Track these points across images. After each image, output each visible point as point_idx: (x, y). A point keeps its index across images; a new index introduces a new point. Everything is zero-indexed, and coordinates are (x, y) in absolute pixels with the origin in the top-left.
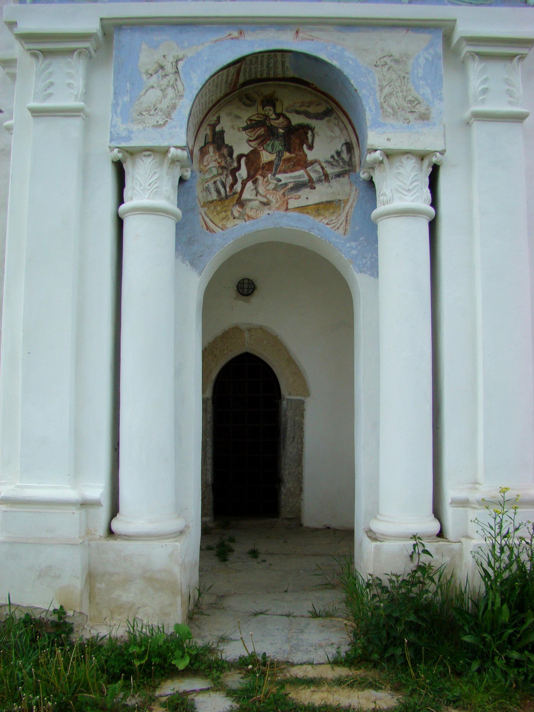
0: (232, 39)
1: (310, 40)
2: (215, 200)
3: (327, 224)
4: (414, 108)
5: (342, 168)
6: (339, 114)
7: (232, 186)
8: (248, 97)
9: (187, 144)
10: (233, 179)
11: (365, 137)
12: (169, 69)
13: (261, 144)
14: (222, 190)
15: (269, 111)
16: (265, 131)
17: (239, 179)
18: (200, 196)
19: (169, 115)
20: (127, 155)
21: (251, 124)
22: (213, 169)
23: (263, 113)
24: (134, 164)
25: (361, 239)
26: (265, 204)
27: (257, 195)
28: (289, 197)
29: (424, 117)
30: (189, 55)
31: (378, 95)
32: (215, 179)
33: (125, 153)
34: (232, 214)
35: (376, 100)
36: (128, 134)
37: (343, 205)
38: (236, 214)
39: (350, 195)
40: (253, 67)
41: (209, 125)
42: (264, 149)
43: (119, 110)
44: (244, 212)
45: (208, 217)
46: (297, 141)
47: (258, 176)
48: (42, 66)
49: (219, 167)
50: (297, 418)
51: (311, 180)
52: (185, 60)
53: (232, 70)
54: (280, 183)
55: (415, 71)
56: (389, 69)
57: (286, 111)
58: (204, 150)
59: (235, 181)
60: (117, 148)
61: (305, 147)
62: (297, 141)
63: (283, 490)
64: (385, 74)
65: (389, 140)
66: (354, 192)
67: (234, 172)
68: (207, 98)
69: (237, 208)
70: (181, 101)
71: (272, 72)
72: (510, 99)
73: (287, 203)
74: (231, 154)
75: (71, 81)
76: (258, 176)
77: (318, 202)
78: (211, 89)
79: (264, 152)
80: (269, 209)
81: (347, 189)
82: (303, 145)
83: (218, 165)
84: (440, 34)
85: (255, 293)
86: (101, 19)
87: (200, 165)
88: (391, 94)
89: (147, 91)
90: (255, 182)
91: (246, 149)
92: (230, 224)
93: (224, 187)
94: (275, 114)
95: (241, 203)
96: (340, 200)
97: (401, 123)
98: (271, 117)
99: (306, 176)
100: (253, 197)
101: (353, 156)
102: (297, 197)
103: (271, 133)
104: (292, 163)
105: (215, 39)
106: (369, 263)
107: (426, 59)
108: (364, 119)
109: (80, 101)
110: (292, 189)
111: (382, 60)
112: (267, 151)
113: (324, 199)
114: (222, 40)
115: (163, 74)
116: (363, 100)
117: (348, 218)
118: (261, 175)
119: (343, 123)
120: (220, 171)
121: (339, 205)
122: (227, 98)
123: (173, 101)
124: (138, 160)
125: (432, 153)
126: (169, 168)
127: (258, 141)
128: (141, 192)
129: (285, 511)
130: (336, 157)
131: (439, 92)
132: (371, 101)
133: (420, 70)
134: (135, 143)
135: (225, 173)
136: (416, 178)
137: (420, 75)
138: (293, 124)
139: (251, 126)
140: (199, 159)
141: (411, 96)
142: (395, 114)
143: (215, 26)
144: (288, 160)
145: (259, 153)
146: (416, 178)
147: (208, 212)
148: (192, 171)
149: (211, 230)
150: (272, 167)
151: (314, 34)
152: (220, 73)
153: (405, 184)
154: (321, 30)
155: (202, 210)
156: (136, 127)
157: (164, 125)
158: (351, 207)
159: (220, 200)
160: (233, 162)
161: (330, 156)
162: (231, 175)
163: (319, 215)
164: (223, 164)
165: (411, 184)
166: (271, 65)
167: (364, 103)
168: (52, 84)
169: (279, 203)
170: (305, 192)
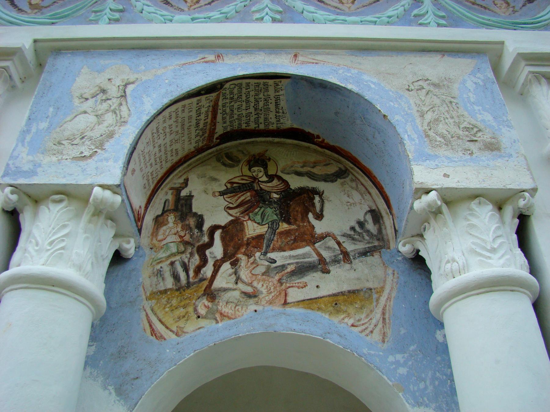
0: (206, 62)
1: (313, 63)
2: (170, 289)
3: (353, 325)
4: (474, 135)
5: (369, 243)
7: (198, 270)
8: (229, 156)
10: (201, 259)
12: (113, 91)
13: (245, 212)
14: (183, 276)
15: (259, 172)
16: (251, 196)
18: (147, 282)
19: (101, 145)
21: (232, 187)
23: (250, 174)
24: (35, 214)
25: (412, 348)
26: (249, 296)
27: (236, 283)
28: (288, 285)
30: (144, 78)
34: (195, 310)
35: (417, 127)
36: (32, 167)
37: (375, 296)
38: (202, 311)
39: (385, 281)
41: (171, 189)
42: (249, 219)
44: (215, 307)
45: (155, 314)
47: (240, 256)
49: (180, 242)
51: (322, 260)
52: (136, 84)
53: (205, 101)
55: (465, 96)
56: (428, 93)
57: (282, 172)
58: (161, 219)
59: (204, 261)
60: (11, 186)
61: (310, 216)
64: (423, 98)
65: (446, 176)
66: (391, 276)
67: (202, 250)
70: (122, 128)
71: (262, 120)
73: (286, 295)
74: (200, 224)
76: (240, 256)
77: (334, 292)
79: (249, 222)
80: (257, 303)
81: (380, 272)
82: (307, 214)
83: (179, 240)
87: (152, 240)
89: (76, 116)
91: (223, 219)
92: (190, 327)
93: (186, 269)
95: (211, 294)
96: (371, 289)
98: (260, 179)
99: (314, 255)
100: (231, 286)
101: (383, 227)
102: (301, 285)
103: (261, 198)
104: (293, 238)
105: (183, 62)
107: (475, 83)
110: (293, 273)
113: (345, 288)
114: (193, 63)
115: (104, 98)
116: (397, 128)
117: (387, 316)
119: (362, 184)
120: (182, 248)
121: (370, 296)
122: (200, 156)
123: (111, 129)
126: (90, 221)
130: (358, 229)
132: (409, 127)
133: (471, 95)
137: (472, 100)
138: (292, 187)
139: (232, 190)
140: (151, 231)
141: (465, 123)
142: (448, 143)
144: (287, 233)
145: (242, 223)
147: (156, 308)
149: (158, 335)
150: (262, 244)
151: (319, 58)
154: (328, 54)
155: (148, 305)
157: (91, 156)
158: (389, 299)
159: (178, 290)
160: (202, 235)
161: (348, 228)
162: (198, 253)
163: (338, 312)
164: (187, 238)
166: (261, 104)
167: (400, 130)
169: (273, 294)
170: (313, 278)
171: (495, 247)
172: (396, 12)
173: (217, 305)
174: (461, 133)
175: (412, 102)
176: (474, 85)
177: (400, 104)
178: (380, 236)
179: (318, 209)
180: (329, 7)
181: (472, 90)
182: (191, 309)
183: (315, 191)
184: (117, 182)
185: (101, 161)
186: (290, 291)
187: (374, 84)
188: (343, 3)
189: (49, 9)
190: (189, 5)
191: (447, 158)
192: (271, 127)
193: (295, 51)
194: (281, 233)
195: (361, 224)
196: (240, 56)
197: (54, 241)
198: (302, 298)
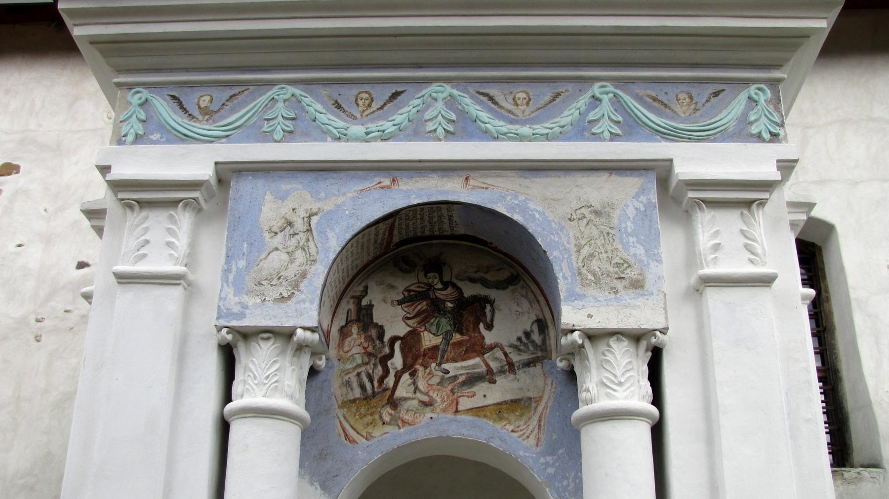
0: (382, 188)
2: (358, 399)
3: (513, 431)
5: (533, 354)
6: (526, 279)
7: (381, 380)
9: (320, 323)
10: (383, 370)
12: (300, 225)
13: (422, 322)
14: (368, 386)
17: (391, 370)
18: (338, 392)
19: (296, 286)
20: (239, 337)
22: (357, 356)
23: (425, 281)
24: (248, 349)
29: (637, 285)
30: (326, 208)
31: (574, 257)
32: (359, 370)
33: (237, 335)
34: (381, 417)
37: (534, 405)
38: (387, 418)
39: (543, 391)
40: (411, 223)
42: (426, 330)
43: (231, 277)
45: (347, 421)
46: (471, 319)
47: (417, 367)
48: (137, 220)
51: (490, 371)
54: (448, 376)
55: (623, 225)
58: (345, 330)
59: (386, 372)
60: (226, 327)
61: (481, 326)
62: (471, 319)
65: (590, 316)
68: (349, 262)
71: (436, 228)
72: (752, 257)
74: (381, 336)
75: (173, 240)
76: (417, 367)
78: (355, 252)
79: (426, 333)
80: (432, 411)
81: (540, 382)
84: (653, 177)
86: (216, 163)
88: (592, 255)
90: (413, 374)
91: (401, 329)
92: (377, 432)
94: (442, 282)
95: (394, 403)
97: (607, 294)
100: (410, 395)
105: (360, 188)
107: (636, 209)
108: (557, 288)
109: (181, 265)
111: (579, 212)
112: (430, 331)
113: (509, 397)
114: (369, 189)
115: (291, 232)
117: (542, 423)
118: (422, 365)
119: (532, 292)
120: (366, 359)
121: (530, 404)
123: (303, 268)
124: (254, 344)
125: (652, 332)
126: (294, 356)
127: (418, 319)
128: (254, 387)
130: (524, 339)
131: (656, 251)
132: (564, 265)
133: (629, 224)
134: (251, 321)
135: (373, 362)
136: (630, 367)
137: (629, 230)
138: (466, 295)
139: (408, 299)
142: (597, 281)
144: (459, 344)
146: (630, 367)
147: (348, 417)
148: (327, 359)
151: (489, 181)
152: (366, 231)
153: (615, 376)
154: (498, 176)
155: (340, 413)
156: (252, 301)
157: (289, 297)
158: (545, 407)
159: (365, 399)
160: (384, 346)
161: (515, 338)
163: (501, 419)
164: (370, 349)
166: (435, 220)
167: (556, 268)
168: (147, 242)
170: (481, 388)
171: (622, 380)
172: (570, 118)
173: (399, 413)
174: (611, 269)
175: (571, 234)
176: (635, 212)
177: (560, 238)
179: (488, 319)
180: (502, 111)
181: (631, 217)
182: (377, 417)
183: (487, 300)
184: (315, 324)
185: (299, 302)
186: (461, 399)
187: (539, 212)
188: (517, 105)
189: (219, 114)
190: (361, 109)
192: (445, 233)
193: (465, 174)
194: (454, 344)
195: (527, 334)
196: (414, 179)
197: (268, 376)
198: (470, 406)
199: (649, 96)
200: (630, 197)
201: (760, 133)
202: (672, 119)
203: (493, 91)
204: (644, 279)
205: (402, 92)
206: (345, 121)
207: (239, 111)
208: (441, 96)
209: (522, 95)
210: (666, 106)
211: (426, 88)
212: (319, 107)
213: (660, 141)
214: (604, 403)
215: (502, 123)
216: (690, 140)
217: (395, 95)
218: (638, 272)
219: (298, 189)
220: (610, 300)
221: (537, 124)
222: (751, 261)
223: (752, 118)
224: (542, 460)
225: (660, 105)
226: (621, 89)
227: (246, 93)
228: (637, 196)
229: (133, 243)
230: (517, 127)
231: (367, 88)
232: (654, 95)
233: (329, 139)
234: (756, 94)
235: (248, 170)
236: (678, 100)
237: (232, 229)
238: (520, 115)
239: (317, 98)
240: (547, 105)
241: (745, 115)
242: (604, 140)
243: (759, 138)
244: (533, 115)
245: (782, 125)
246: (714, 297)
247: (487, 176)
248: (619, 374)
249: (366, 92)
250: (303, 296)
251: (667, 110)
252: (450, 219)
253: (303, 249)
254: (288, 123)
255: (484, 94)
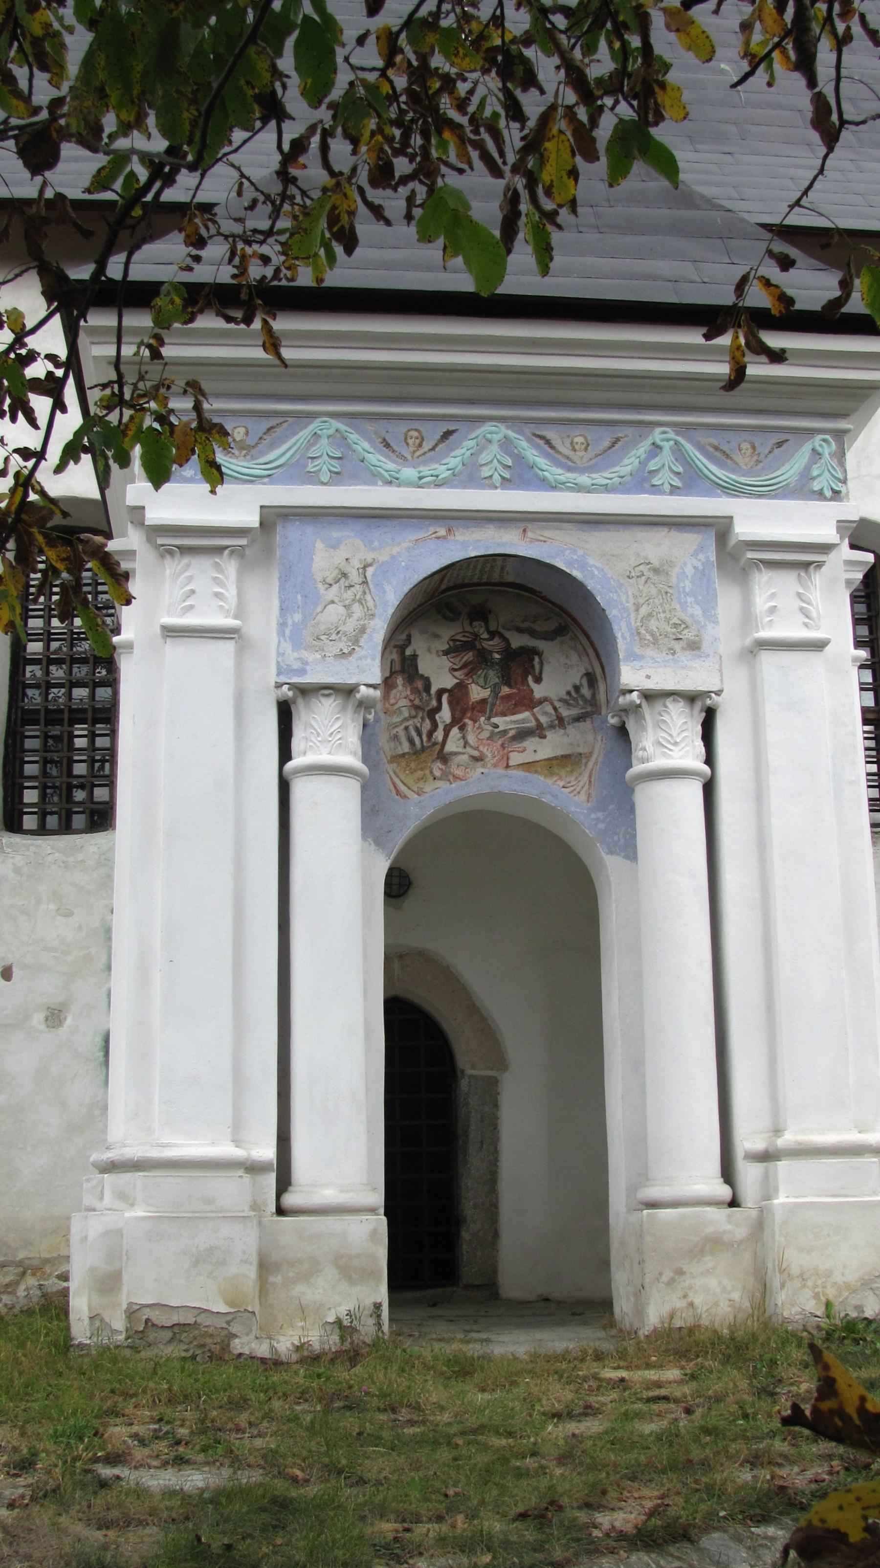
0: (438, 538)
7: (430, 734)
11: (617, 673)
12: (355, 577)
14: (417, 740)
19: (356, 641)
20: (298, 693)
29: (694, 646)
31: (633, 615)
32: (407, 724)
34: (431, 772)
37: (584, 761)
38: (437, 773)
43: (288, 632)
50: (487, 1109)
51: (539, 726)
52: (375, 566)
54: (497, 730)
57: (504, 628)
58: (390, 682)
59: (435, 726)
61: (530, 679)
63: (465, 1235)
64: (641, 587)
65: (648, 677)
69: (439, 764)
72: (807, 620)
76: (466, 720)
77: (550, 756)
80: (483, 766)
81: (590, 737)
84: (713, 534)
85: (411, 892)
86: (261, 507)
88: (650, 615)
90: (462, 728)
91: (449, 682)
92: (428, 788)
93: (420, 734)
94: (489, 632)
100: (460, 750)
106: (622, 841)
111: (637, 569)
112: (477, 684)
113: (559, 753)
114: (424, 539)
118: (471, 719)
119: (581, 643)
120: (413, 713)
121: (580, 760)
126: (355, 712)
129: (469, 1272)
132: (623, 624)
133: (687, 583)
135: (420, 715)
136: (685, 727)
137: (687, 590)
139: (454, 649)
142: (655, 642)
143: (415, 521)
144: (508, 697)
146: (685, 727)
151: (547, 533)
154: (557, 529)
155: (390, 768)
156: (312, 657)
157: (350, 653)
158: (596, 764)
159: (415, 753)
160: (431, 699)
163: (552, 774)
164: (417, 702)
165: (679, 734)
167: (615, 627)
170: (531, 743)
174: (669, 629)
177: (619, 596)
178: (593, 702)
180: (560, 457)
181: (690, 575)
182: (427, 772)
185: (360, 659)
188: (575, 451)
190: (411, 449)
191: (653, 658)
193: (522, 525)
194: (503, 697)
195: (577, 688)
199: (711, 445)
200: (688, 553)
201: (822, 489)
202: (733, 471)
203: (550, 433)
204: (700, 641)
205: (453, 432)
206: (395, 462)
207: (280, 446)
208: (496, 437)
209: (580, 439)
210: (727, 456)
211: (479, 427)
212: (366, 445)
213: (719, 496)
214: (660, 762)
215: (559, 471)
216: (751, 495)
217: (447, 435)
218: (695, 633)
219: (349, 537)
220: (668, 661)
221: (596, 472)
222: (806, 625)
223: (815, 473)
224: (593, 816)
225: (722, 456)
226: (684, 437)
227: (285, 425)
228: (695, 554)
229: (180, 593)
230: (575, 475)
231: (416, 425)
232: (716, 443)
233: (380, 483)
234: (821, 446)
235: (294, 515)
236: (740, 450)
237: (284, 580)
238: (578, 462)
239: (363, 434)
240: (605, 451)
241: (808, 469)
242: (663, 493)
243: (820, 495)
244: (592, 462)
245: (844, 481)
246: (769, 661)
247: (545, 528)
248: (674, 734)
249: (416, 430)
250: (364, 653)
251: (729, 461)
252: (502, 569)
253: (360, 601)
254: (333, 462)
255: (539, 436)
